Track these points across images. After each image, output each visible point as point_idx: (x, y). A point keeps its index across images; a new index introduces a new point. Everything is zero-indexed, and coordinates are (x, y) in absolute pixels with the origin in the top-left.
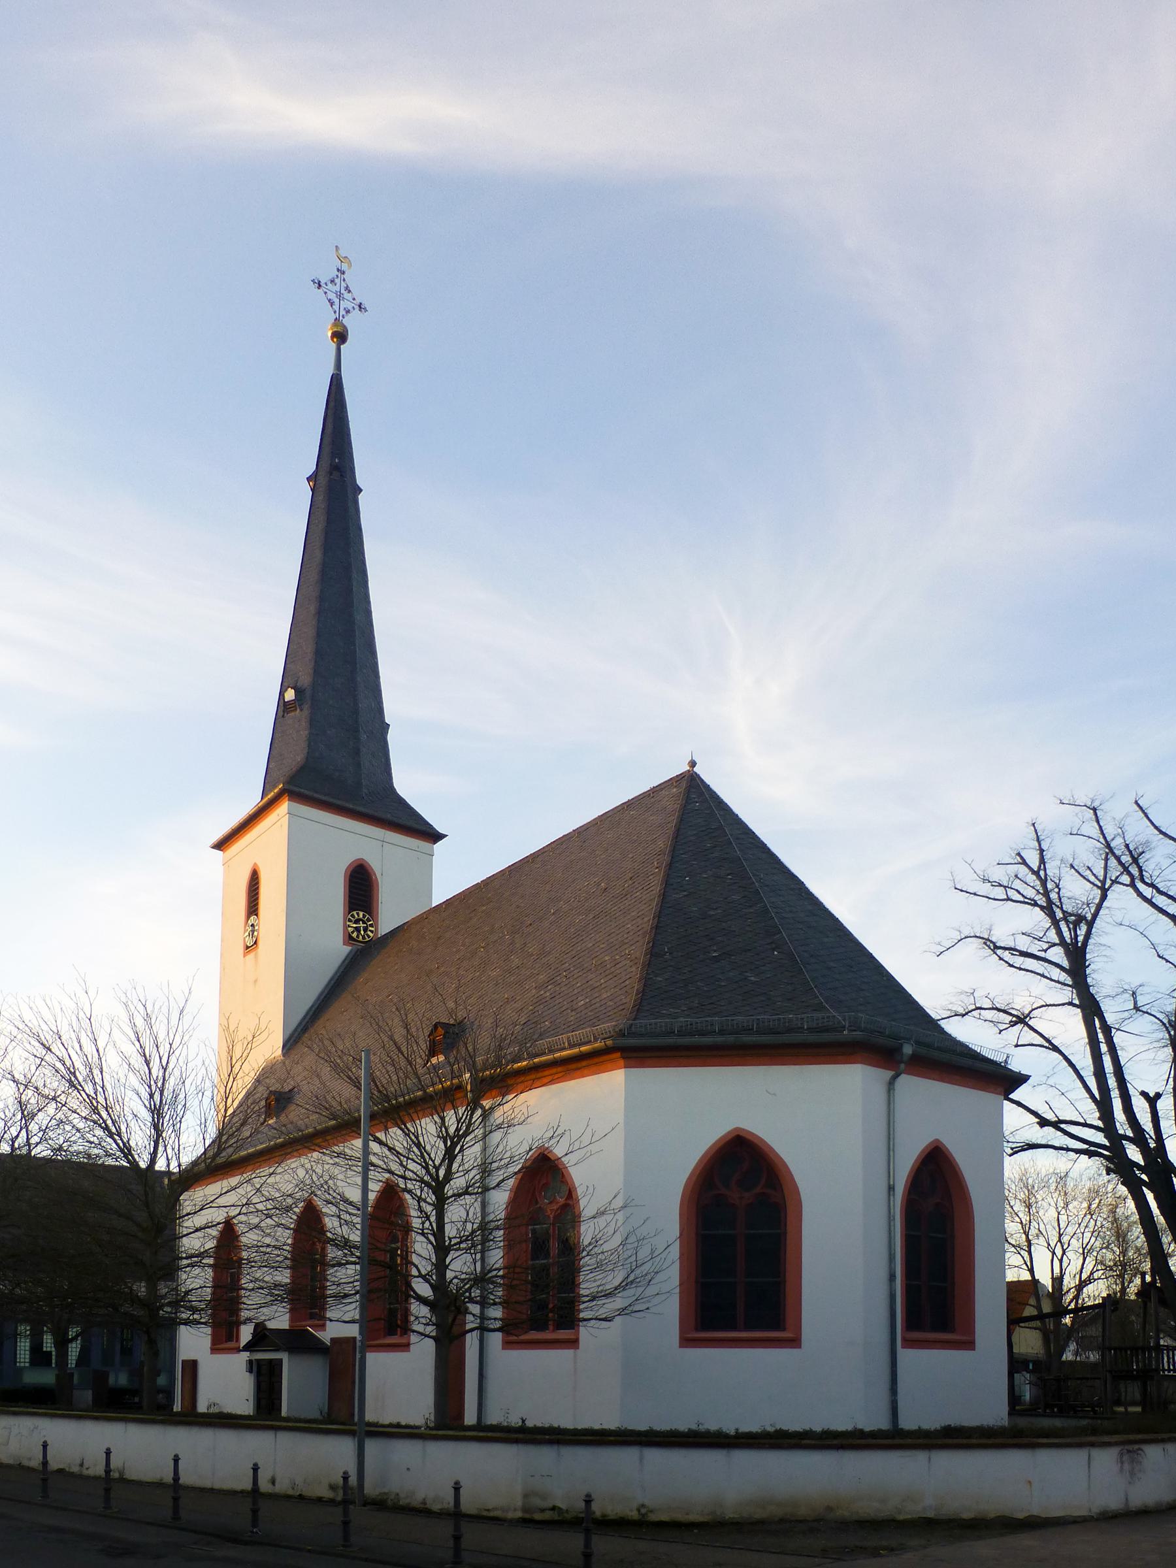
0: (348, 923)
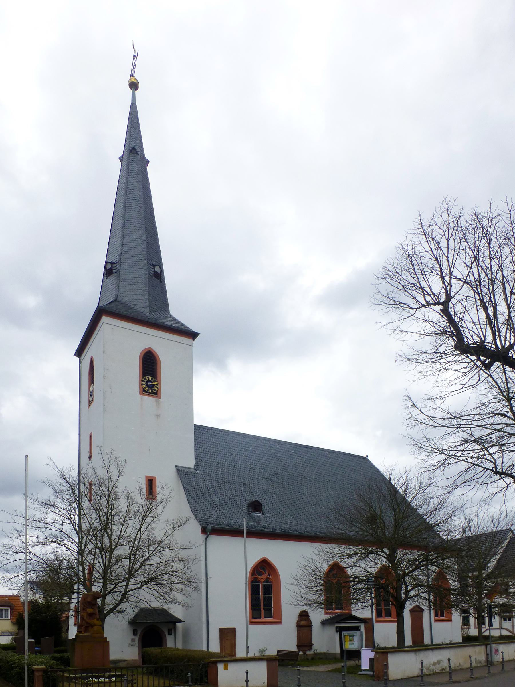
0: (143, 383)
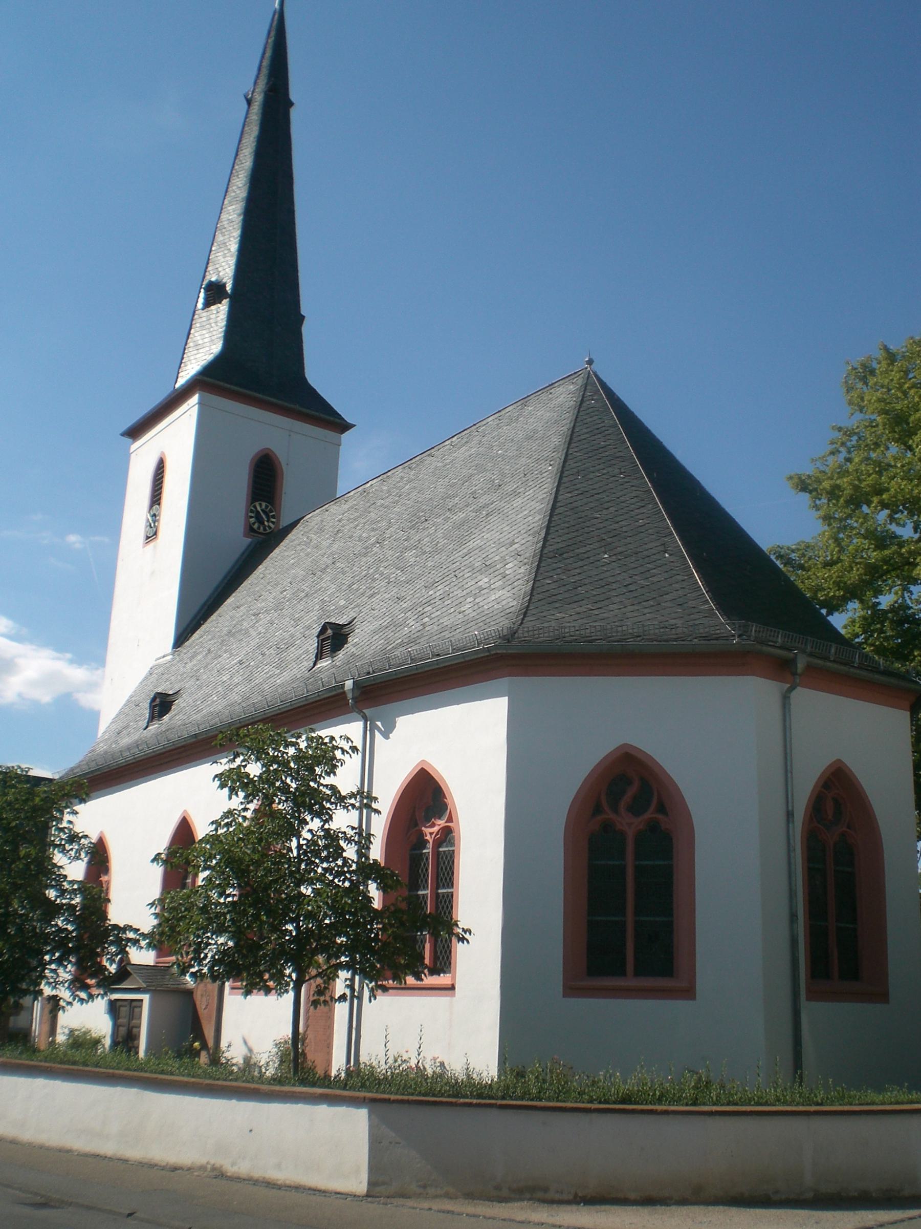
0: (250, 514)
